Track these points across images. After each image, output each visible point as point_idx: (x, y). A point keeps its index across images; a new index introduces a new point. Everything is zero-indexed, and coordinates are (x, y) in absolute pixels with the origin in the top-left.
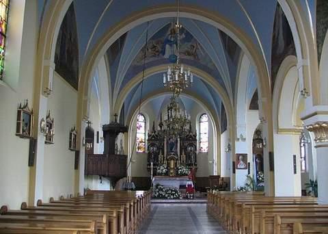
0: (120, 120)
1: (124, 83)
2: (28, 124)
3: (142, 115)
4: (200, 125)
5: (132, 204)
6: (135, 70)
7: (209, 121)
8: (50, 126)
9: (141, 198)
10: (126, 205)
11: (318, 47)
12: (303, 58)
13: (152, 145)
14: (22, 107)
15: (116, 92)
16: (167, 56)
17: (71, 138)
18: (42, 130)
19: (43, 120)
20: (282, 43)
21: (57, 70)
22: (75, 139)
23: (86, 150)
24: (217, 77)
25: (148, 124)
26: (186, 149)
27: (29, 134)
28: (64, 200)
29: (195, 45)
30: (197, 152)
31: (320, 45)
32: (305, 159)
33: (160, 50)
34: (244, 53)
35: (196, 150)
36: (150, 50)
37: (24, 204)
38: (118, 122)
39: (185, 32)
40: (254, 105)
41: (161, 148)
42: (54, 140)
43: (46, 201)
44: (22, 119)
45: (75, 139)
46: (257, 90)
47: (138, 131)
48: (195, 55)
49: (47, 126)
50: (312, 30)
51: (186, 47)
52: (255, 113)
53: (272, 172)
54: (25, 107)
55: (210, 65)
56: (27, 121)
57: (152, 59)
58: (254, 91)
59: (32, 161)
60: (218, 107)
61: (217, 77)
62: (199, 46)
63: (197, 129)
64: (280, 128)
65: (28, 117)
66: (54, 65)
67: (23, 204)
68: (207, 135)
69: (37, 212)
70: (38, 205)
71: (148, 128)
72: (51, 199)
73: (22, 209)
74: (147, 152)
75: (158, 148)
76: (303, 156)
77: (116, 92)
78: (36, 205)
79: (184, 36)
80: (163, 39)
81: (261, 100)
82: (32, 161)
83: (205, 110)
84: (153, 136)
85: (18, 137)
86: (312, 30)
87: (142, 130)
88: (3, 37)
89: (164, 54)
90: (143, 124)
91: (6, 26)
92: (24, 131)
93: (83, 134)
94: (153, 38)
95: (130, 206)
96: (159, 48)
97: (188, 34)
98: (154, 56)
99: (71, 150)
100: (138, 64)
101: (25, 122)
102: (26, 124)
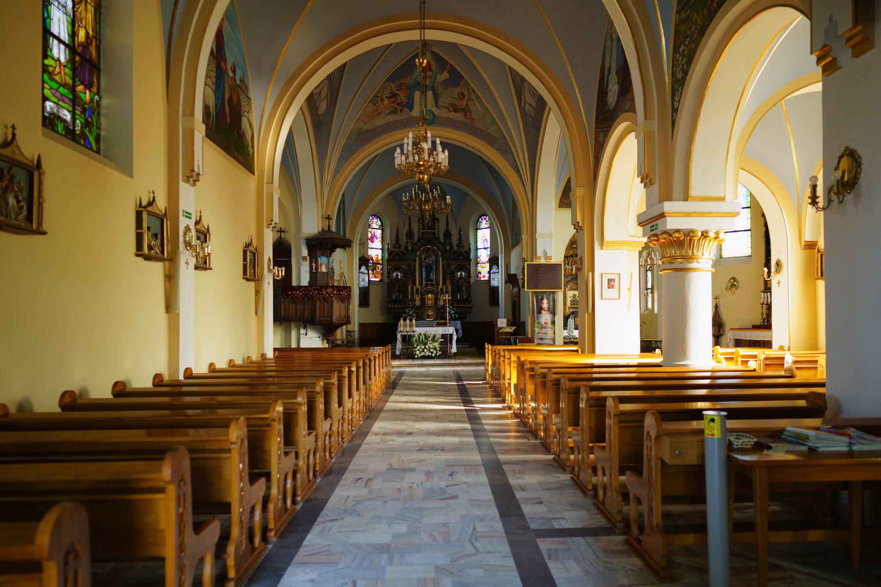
0: (338, 227)
1: (348, 153)
2: (159, 236)
3: (378, 217)
4: (476, 235)
5: (354, 369)
6: (362, 138)
7: (491, 227)
8: (204, 236)
9: (675, 452)
10: (341, 372)
11: (673, 96)
12: (646, 118)
13: (396, 269)
14: (144, 203)
15: (328, 177)
16: (416, 113)
17: (245, 259)
18: (188, 244)
19: (188, 229)
20: (613, 88)
21: (208, 135)
22: (254, 260)
23: (274, 280)
24: (506, 150)
25: (388, 232)
26: (453, 274)
27: (163, 252)
28: (234, 366)
29: (466, 94)
30: (472, 280)
31: (677, 98)
32: (652, 292)
33: (405, 101)
34: (550, 110)
35: (470, 276)
36: (386, 101)
37: (158, 378)
38: (334, 229)
39: (448, 67)
40: (565, 200)
41: (409, 274)
42: (214, 262)
43: (201, 369)
44: (145, 225)
45: (254, 260)
46: (570, 178)
47: (371, 245)
48: (466, 111)
49: (198, 238)
50: (665, 65)
51: (449, 96)
52: (567, 213)
53: (751, 327)
54: (150, 204)
55: (492, 131)
56: (156, 229)
57: (392, 118)
58: (567, 179)
59: (170, 305)
60: (507, 207)
61: (506, 150)
62: (473, 95)
63: (472, 241)
64: (478, 248)
65: (158, 222)
66: (203, 127)
67: (156, 375)
68: (488, 252)
69: (185, 389)
70: (185, 378)
71: (388, 240)
72: (211, 365)
73: (154, 385)
74: (386, 280)
75: (405, 274)
76: (649, 286)
77: (328, 177)
78: (181, 377)
79: (446, 75)
80: (410, 80)
81: (578, 192)
82: (170, 305)
83: (487, 209)
84: (397, 253)
85: (140, 259)
86: (665, 65)
87: (377, 244)
88: (95, 71)
89: (411, 108)
90: (378, 233)
91: (98, 48)
92: (150, 248)
93: (268, 252)
94: (390, 79)
95: (350, 372)
96: (402, 98)
97: (453, 72)
98: (394, 112)
99: (248, 280)
100: (366, 127)
101: (153, 231)
102: (156, 235)
